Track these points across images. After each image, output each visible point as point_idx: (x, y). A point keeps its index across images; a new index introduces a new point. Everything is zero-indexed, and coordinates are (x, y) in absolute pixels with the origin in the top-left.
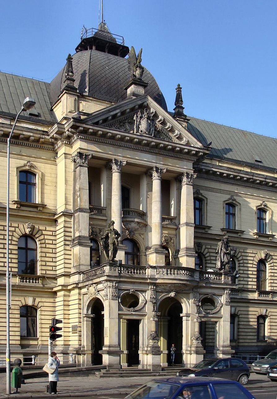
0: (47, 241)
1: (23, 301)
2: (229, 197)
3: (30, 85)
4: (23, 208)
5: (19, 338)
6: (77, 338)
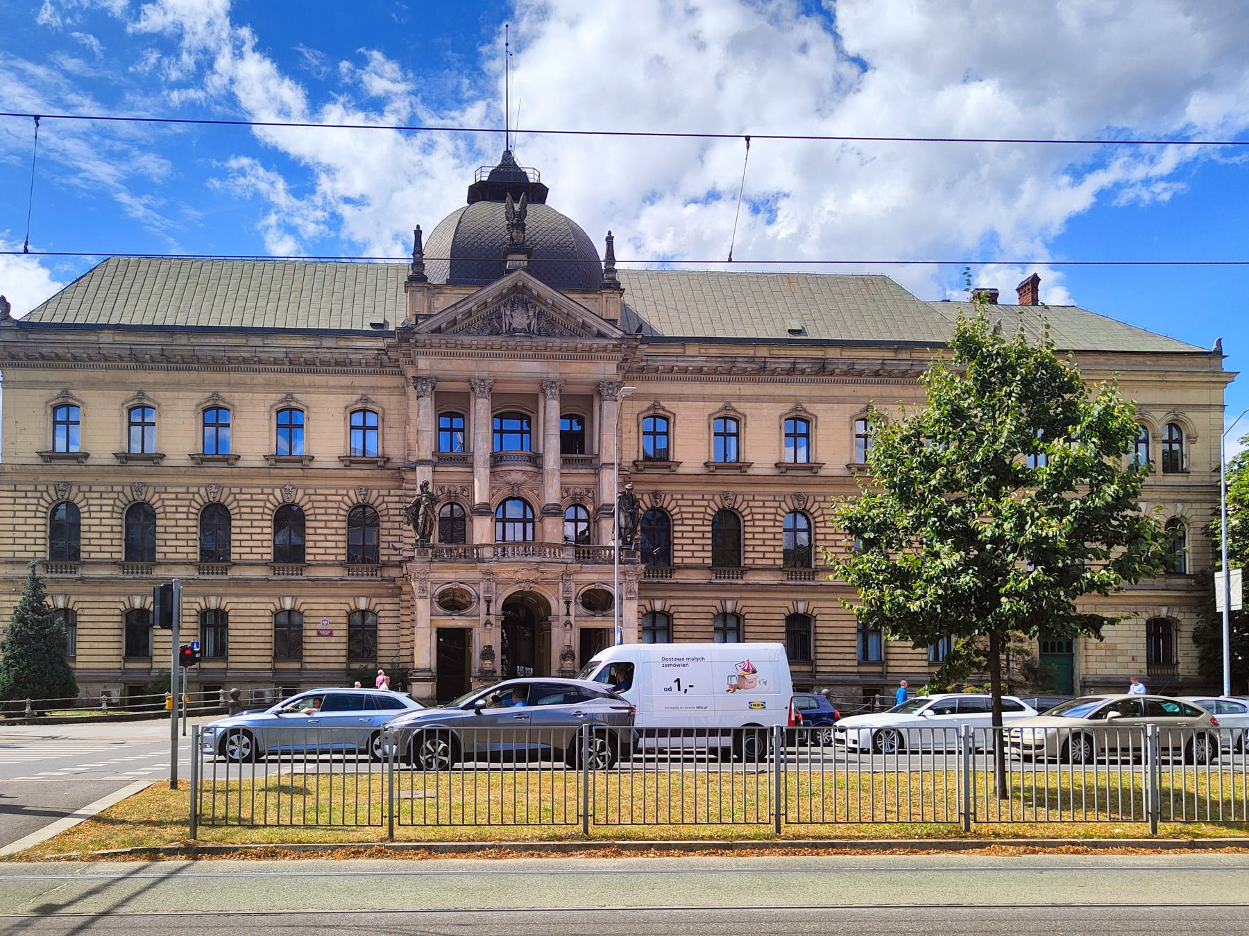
0: (318, 511)
1: (352, 605)
2: (721, 405)
4: (353, 466)
5: (344, 659)
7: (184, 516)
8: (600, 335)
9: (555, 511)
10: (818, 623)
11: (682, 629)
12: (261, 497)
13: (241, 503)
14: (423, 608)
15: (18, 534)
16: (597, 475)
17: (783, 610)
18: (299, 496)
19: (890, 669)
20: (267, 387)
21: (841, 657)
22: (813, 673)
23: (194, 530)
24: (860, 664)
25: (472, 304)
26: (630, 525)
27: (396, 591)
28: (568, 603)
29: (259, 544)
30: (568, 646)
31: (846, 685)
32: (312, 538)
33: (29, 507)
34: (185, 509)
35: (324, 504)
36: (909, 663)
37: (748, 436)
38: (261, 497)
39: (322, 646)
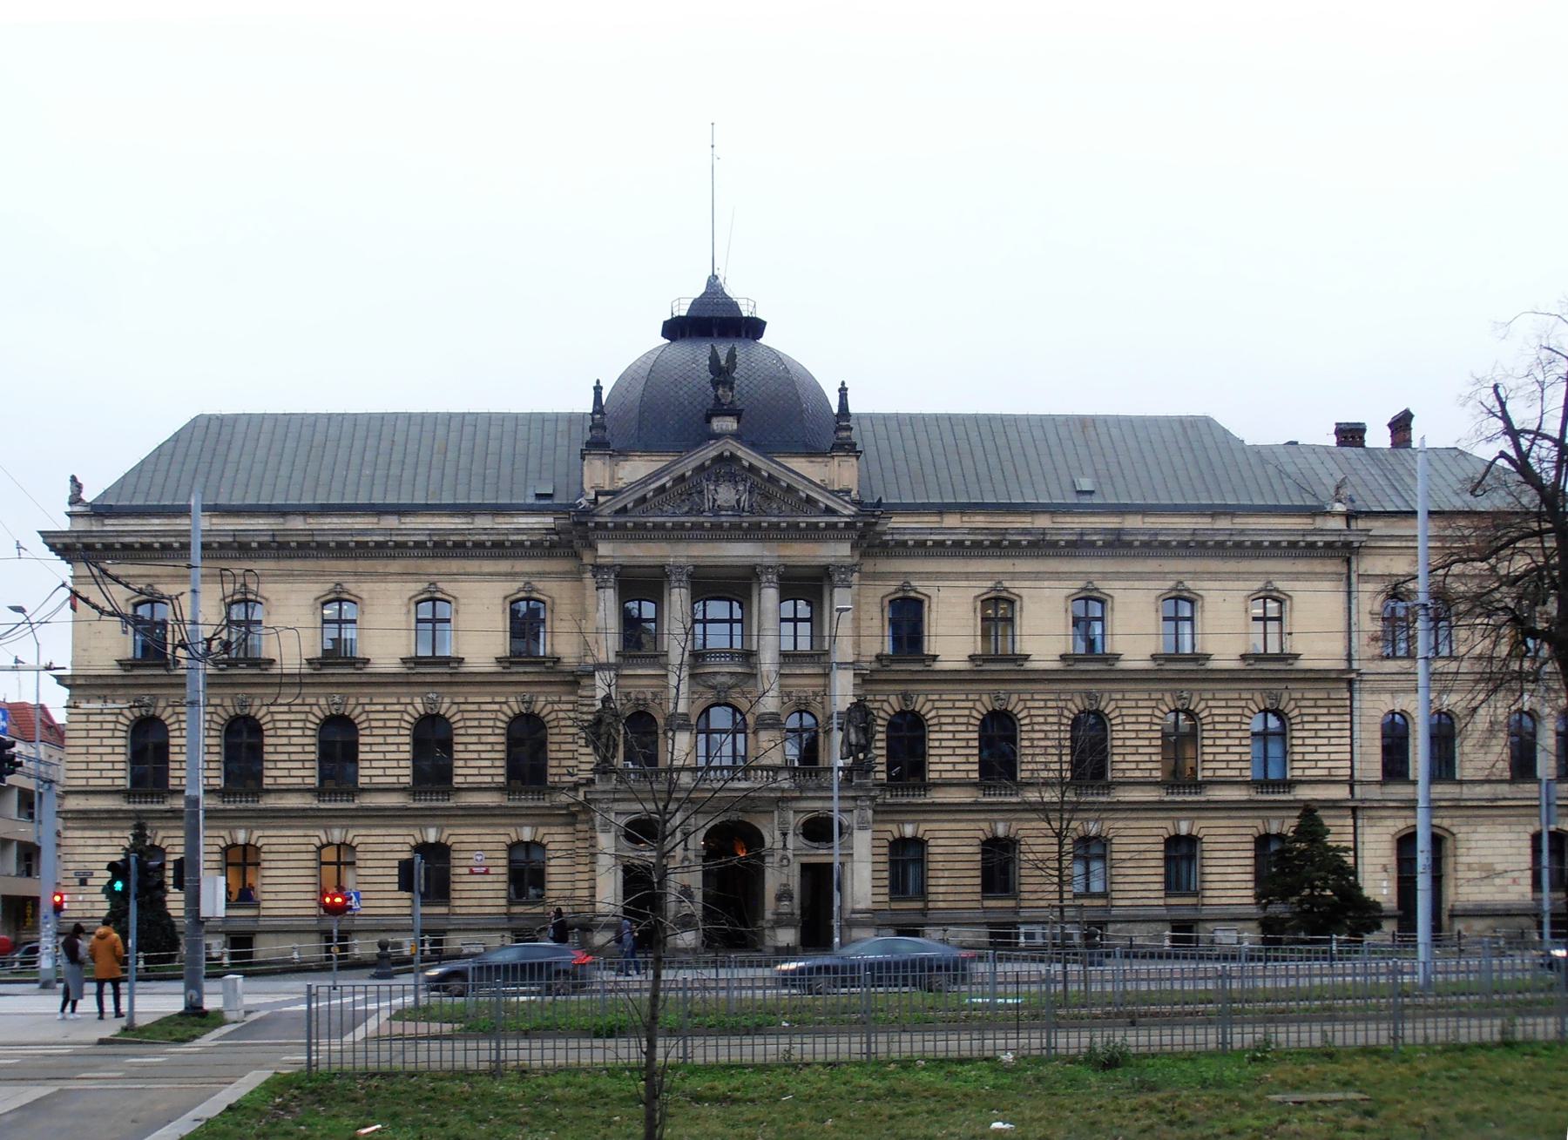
3: (1271, 470)
5: (503, 902)
7: (299, 732)
8: (829, 511)
9: (771, 722)
10: (1115, 848)
11: (940, 858)
12: (397, 707)
13: (372, 716)
14: (606, 841)
15: (92, 758)
16: (826, 675)
17: (1161, 831)
18: (445, 706)
19: (1206, 901)
21: (1142, 887)
22: (924, 912)
23: (312, 749)
25: (667, 478)
26: (863, 741)
27: (569, 819)
28: (785, 834)
29: (394, 764)
30: (785, 885)
31: (1149, 921)
32: (461, 755)
33: (106, 726)
34: (300, 724)
35: (477, 715)
36: (1230, 893)
37: (1025, 622)
38: (397, 707)
39: (476, 886)
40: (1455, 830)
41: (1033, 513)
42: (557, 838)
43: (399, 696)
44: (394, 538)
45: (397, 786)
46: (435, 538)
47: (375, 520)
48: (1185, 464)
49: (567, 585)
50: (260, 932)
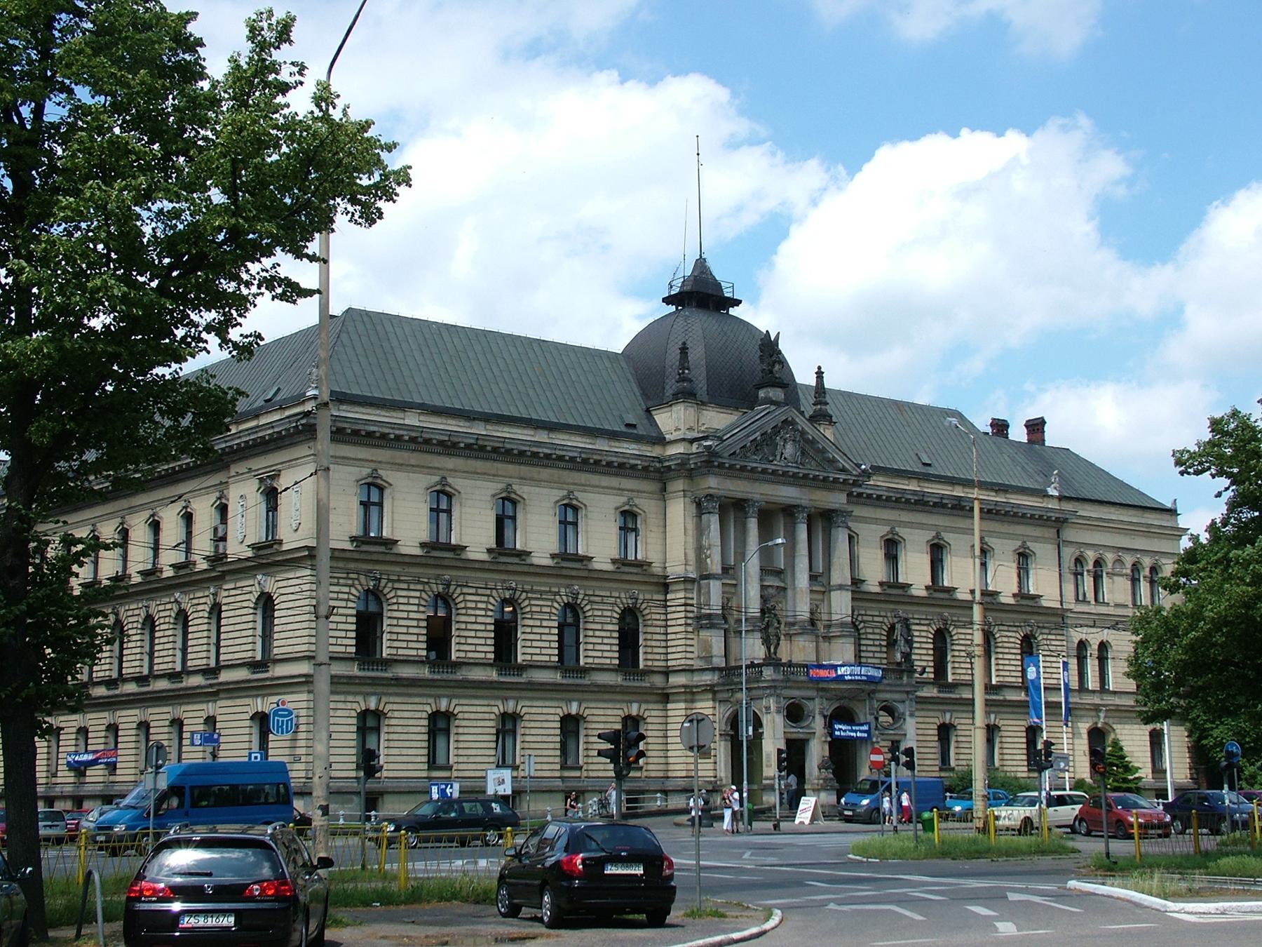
2: (888, 529)
6: (711, 766)
8: (844, 470)
20: (550, 483)
24: (941, 770)
40: (1115, 726)
41: (1006, 491)
42: (654, 713)
43: (611, 590)
44: (558, 452)
45: (549, 664)
46: (583, 456)
47: (532, 432)
48: (419, 345)
49: (653, 503)
50: (588, 791)
